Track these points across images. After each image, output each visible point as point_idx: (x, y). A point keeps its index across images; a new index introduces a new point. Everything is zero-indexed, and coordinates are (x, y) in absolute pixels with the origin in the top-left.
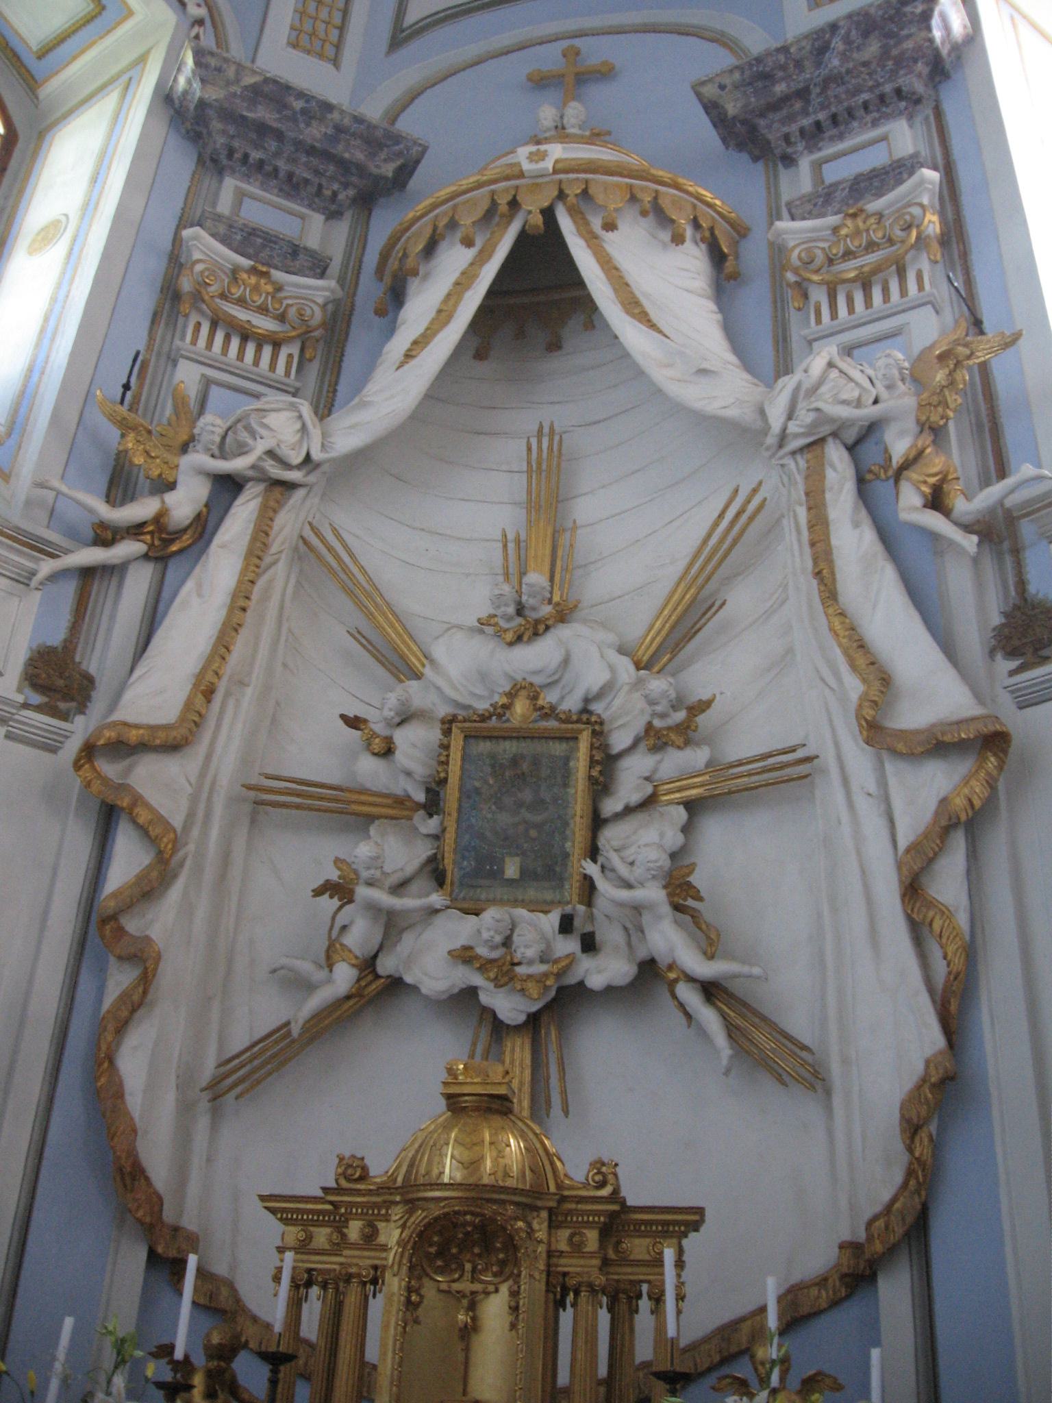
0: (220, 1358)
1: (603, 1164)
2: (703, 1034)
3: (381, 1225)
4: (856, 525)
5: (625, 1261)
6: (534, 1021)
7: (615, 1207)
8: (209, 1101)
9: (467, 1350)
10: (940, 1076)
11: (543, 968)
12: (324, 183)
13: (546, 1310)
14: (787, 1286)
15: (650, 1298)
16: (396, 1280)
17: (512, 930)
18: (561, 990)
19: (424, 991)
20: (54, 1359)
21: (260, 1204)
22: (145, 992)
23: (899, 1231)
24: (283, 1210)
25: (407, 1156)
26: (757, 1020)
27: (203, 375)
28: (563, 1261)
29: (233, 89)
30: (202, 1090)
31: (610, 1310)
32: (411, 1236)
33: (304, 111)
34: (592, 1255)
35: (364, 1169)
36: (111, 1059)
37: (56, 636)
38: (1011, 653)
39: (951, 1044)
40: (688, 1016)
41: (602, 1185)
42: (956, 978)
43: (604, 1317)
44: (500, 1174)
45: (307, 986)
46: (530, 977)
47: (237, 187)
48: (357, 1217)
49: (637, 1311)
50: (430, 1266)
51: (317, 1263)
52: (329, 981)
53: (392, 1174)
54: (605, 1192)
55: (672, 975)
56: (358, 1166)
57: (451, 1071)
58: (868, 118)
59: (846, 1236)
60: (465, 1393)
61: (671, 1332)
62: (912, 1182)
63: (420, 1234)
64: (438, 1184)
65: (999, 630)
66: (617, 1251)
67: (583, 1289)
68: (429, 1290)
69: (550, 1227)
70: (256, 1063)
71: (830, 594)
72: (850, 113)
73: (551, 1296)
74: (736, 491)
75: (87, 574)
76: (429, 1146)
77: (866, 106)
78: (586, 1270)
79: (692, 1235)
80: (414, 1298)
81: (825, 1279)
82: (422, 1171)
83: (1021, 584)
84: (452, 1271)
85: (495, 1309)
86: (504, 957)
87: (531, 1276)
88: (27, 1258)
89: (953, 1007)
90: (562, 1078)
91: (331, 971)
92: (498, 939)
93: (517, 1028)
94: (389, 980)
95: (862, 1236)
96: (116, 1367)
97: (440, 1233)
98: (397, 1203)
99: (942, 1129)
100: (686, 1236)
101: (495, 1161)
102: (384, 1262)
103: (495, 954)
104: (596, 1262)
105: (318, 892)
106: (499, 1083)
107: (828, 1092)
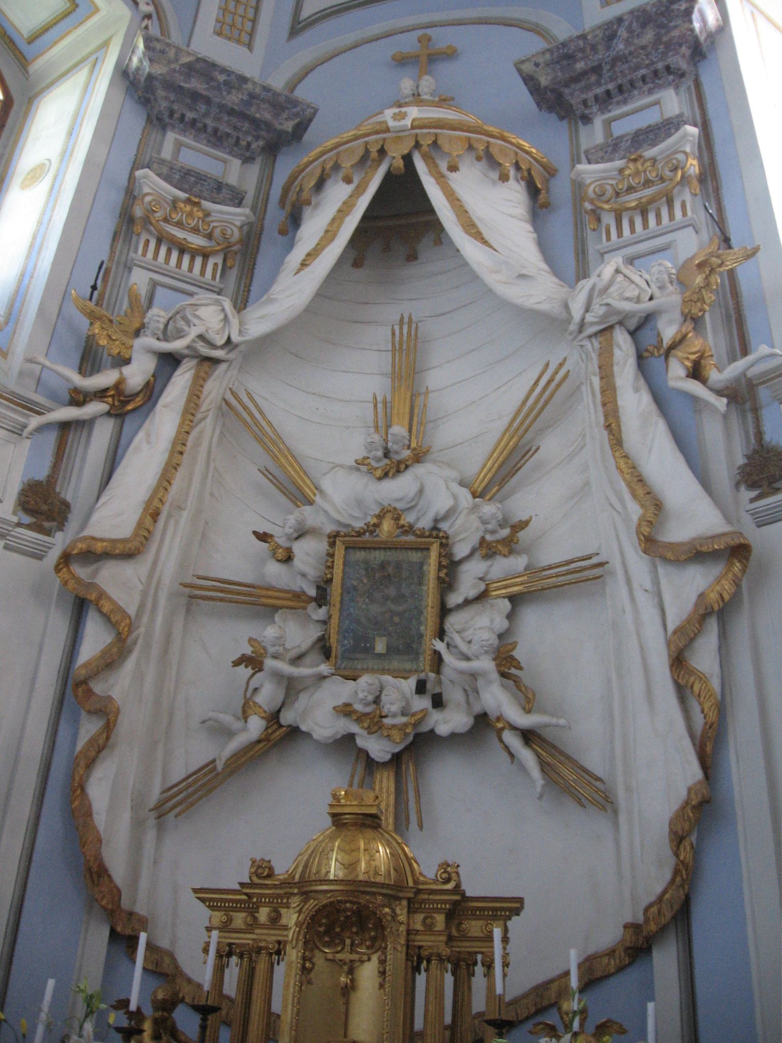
0: (164, 1009)
1: (448, 865)
2: (523, 769)
3: (283, 911)
4: (637, 390)
5: (465, 937)
6: (397, 759)
7: (457, 898)
8: (155, 819)
9: (347, 1003)
10: (699, 800)
11: (404, 720)
12: (241, 136)
13: (406, 974)
14: (585, 956)
15: (483, 965)
16: (294, 951)
17: (381, 692)
18: (417, 736)
19: (315, 736)
20: (40, 1010)
21: (193, 895)
22: (108, 738)
23: (669, 915)
24: (211, 900)
25: (302, 859)
26: (562, 758)
27: (151, 279)
28: (418, 937)
29: (173, 66)
30: (150, 810)
31: (454, 974)
32: (306, 919)
33: (226, 83)
34: (440, 933)
35: (271, 869)
36: (82, 787)
37: (42, 473)
38: (752, 486)
39: (707, 776)
40: (512, 755)
41: (447, 881)
42: (710, 727)
43: (449, 979)
44: (372, 873)
45: (228, 733)
46: (394, 726)
47: (176, 139)
48: (266, 904)
49: (473, 975)
50: (320, 941)
51: (236, 939)
52: (245, 729)
53: (292, 873)
54: (450, 886)
55: (500, 725)
56: (266, 867)
57: (335, 796)
58: (646, 88)
59: (629, 919)
60: (345, 1035)
61: (499, 990)
62: (678, 879)
63: (313, 918)
64: (325, 881)
65: (742, 468)
66: (458, 930)
67: (434, 958)
68: (319, 959)
69: (409, 912)
70: (190, 790)
71: (617, 441)
72: (632, 84)
73: (410, 963)
74: (547, 365)
75: (65, 426)
76: (319, 852)
77: (643, 79)
78: (435, 944)
79: (515, 918)
80: (308, 965)
81: (614, 951)
82: (314, 870)
83: (759, 434)
84: (336, 945)
85: (368, 973)
86: (374, 711)
87: (395, 949)
88: (20, 935)
89: (709, 749)
90: (418, 802)
91: (246, 722)
92: (370, 698)
93: (385, 764)
94: (289, 728)
95: (641, 919)
96: (86, 1017)
97: (327, 917)
98: (295, 894)
99: (700, 839)
100: (510, 919)
101: (368, 863)
102: (286, 939)
103: (368, 710)
104: (443, 938)
105: (236, 663)
106: (371, 805)
107: (616, 812)
